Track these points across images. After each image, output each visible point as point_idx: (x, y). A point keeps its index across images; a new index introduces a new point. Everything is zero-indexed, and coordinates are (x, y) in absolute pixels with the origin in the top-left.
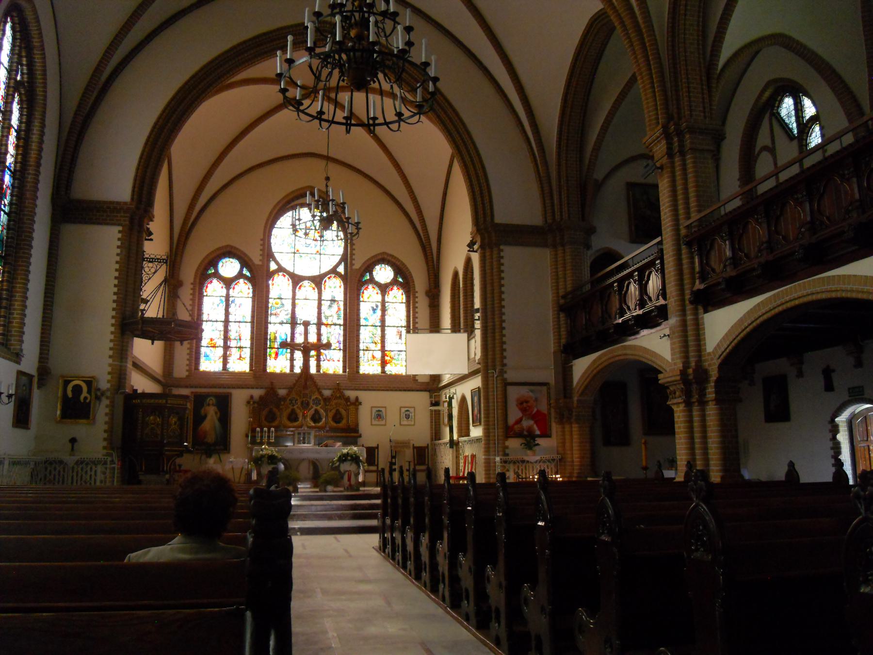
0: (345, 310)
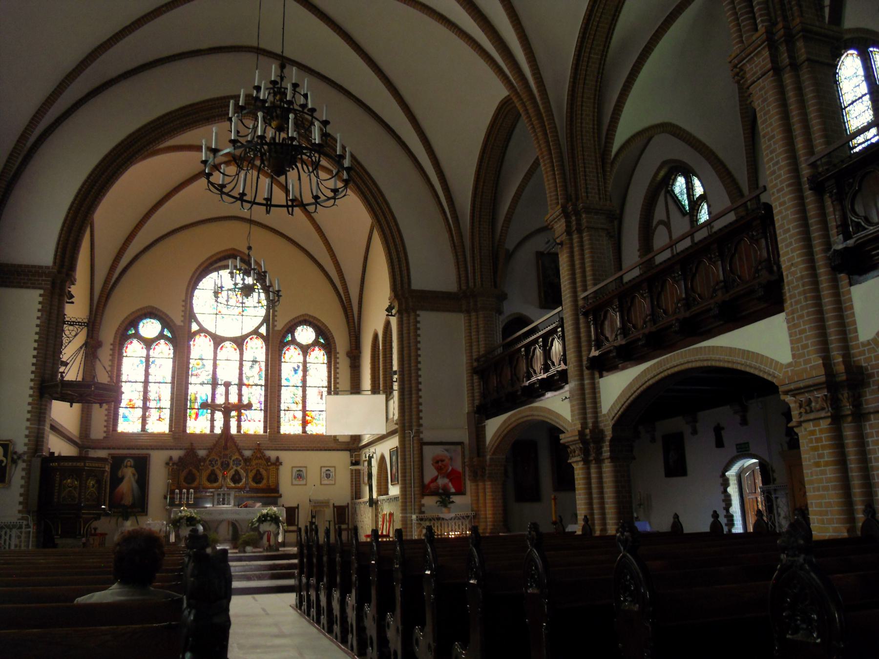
0: (267, 370)
